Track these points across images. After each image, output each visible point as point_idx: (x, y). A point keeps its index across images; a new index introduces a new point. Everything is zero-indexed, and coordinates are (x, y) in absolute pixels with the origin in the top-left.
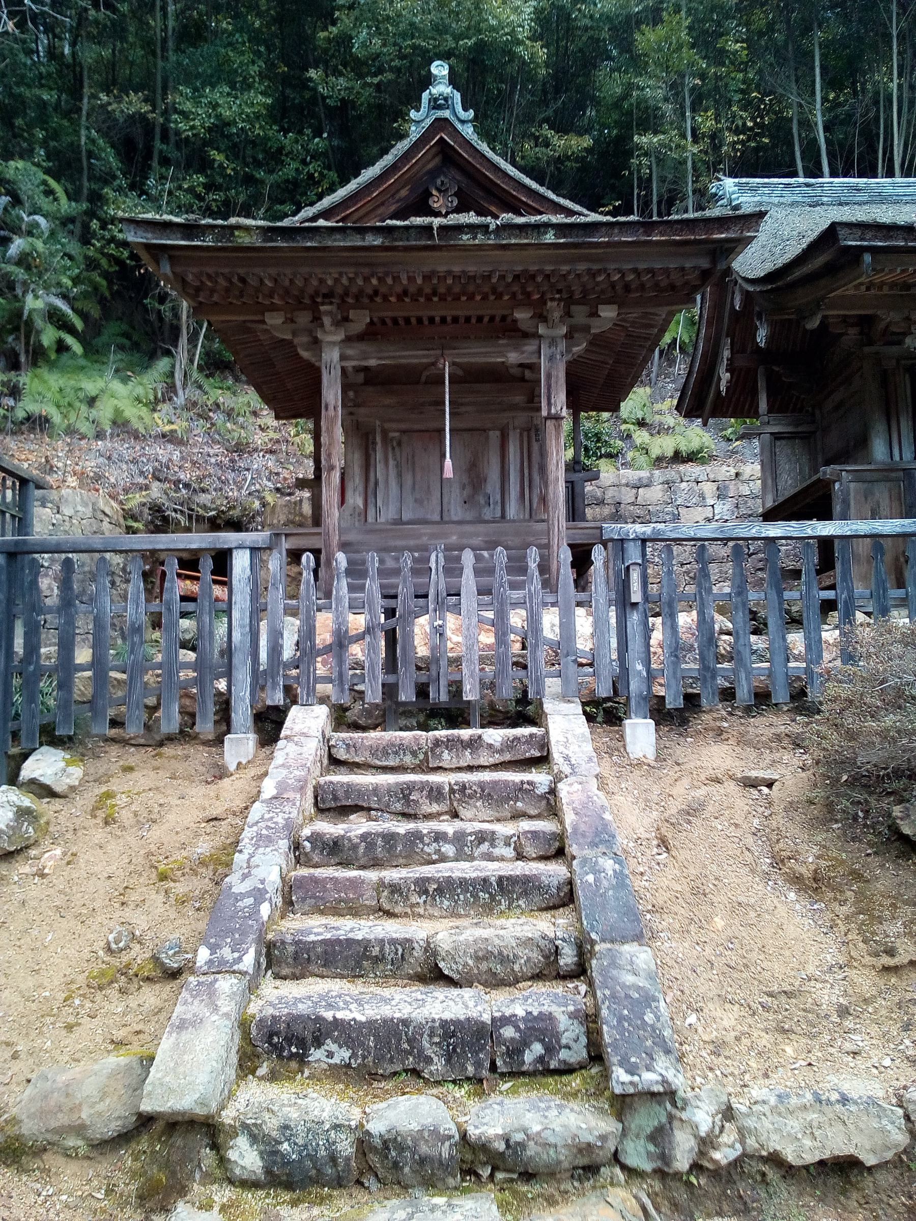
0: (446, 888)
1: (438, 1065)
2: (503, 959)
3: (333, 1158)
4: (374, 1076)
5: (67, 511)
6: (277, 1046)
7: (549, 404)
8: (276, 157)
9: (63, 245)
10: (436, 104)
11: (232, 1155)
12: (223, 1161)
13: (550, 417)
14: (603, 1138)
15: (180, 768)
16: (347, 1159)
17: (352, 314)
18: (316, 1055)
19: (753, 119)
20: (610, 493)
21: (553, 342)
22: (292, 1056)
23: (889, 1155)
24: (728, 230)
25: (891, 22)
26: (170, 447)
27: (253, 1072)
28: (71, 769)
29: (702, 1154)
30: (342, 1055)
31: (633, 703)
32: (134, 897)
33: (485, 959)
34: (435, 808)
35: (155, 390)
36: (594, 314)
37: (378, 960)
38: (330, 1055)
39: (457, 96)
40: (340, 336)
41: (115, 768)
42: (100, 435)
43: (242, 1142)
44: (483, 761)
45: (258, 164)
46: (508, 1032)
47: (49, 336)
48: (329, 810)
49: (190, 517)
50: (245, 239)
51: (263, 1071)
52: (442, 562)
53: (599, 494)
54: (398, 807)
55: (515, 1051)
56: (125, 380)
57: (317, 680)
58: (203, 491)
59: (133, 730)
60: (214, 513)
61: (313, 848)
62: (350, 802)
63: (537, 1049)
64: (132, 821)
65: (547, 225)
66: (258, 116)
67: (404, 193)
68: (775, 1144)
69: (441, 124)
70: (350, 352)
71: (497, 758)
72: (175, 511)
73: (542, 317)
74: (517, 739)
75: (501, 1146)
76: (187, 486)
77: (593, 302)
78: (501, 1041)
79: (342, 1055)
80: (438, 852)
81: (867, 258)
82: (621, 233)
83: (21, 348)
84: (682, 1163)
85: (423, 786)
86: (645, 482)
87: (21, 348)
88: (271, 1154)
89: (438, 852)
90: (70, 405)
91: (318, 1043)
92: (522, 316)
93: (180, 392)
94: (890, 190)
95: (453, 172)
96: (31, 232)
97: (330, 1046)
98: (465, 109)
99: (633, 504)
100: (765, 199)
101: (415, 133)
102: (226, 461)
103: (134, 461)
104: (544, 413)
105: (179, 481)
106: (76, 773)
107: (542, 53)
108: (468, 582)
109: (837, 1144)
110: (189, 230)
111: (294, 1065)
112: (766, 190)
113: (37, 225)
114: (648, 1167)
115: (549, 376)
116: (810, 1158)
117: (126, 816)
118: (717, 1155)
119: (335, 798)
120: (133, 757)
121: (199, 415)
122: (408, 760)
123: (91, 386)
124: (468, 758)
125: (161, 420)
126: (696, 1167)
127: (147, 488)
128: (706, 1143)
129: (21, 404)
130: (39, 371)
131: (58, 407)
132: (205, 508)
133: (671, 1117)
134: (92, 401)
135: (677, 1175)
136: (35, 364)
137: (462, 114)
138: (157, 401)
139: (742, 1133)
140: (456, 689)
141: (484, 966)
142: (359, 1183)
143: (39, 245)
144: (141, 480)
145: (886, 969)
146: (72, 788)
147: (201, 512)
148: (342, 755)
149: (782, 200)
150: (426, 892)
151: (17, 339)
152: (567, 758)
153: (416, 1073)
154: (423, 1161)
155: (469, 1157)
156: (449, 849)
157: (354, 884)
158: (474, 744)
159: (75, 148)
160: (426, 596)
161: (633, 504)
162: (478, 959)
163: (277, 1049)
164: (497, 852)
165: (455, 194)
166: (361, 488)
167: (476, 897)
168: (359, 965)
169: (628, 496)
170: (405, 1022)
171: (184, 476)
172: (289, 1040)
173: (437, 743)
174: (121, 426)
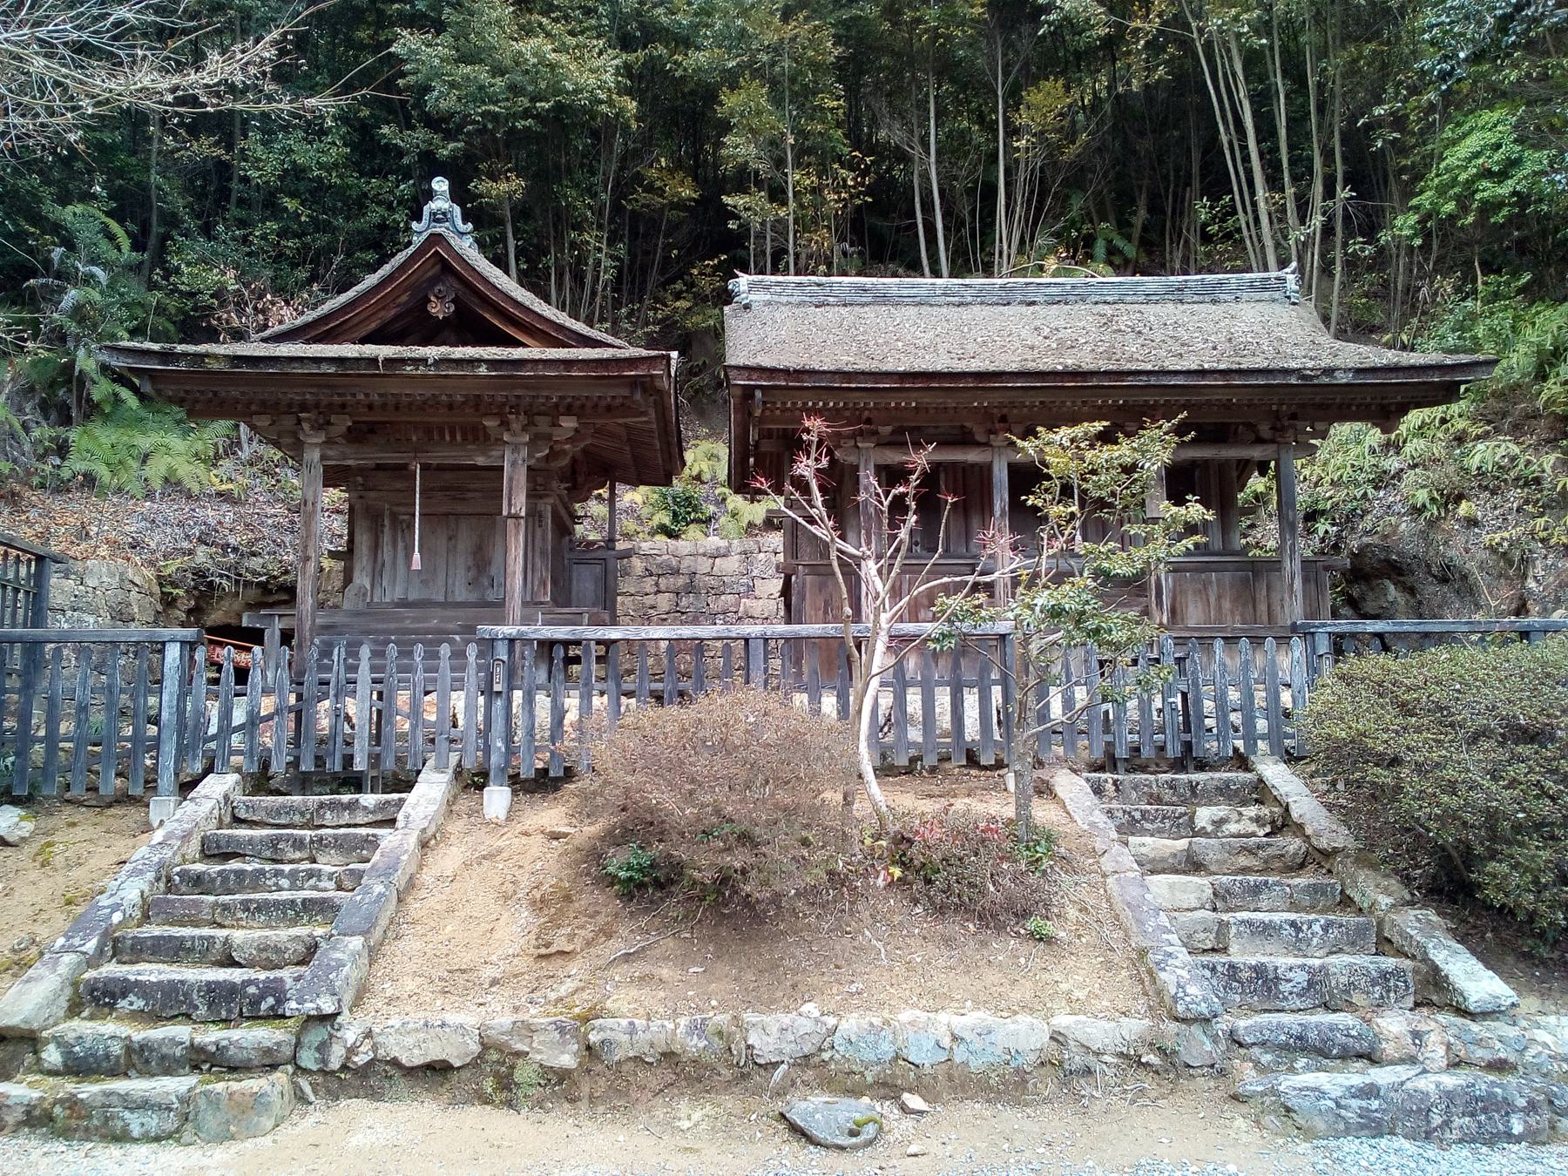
0: (262, 907)
1: (203, 1011)
2: (277, 950)
3: (107, 1056)
4: (160, 1018)
5: (91, 582)
6: (97, 998)
7: (510, 505)
8: (359, 204)
9: (121, 295)
10: (436, 218)
11: (44, 1055)
12: (39, 1060)
13: (510, 516)
14: (278, 1044)
15: (115, 824)
16: (118, 1057)
17: (333, 418)
18: (122, 1003)
19: (854, 179)
20: (686, 563)
21: (516, 449)
22: (106, 1004)
23: (468, 1060)
24: (636, 369)
25: (996, 79)
26: (225, 507)
27: (78, 1015)
28: (23, 824)
29: (348, 1058)
30: (139, 1004)
31: (492, 774)
32: (45, 916)
33: (265, 950)
34: (298, 855)
35: (216, 445)
36: (555, 424)
37: (191, 950)
38: (131, 1004)
39: (457, 210)
40: (321, 438)
41: (61, 824)
42: (149, 496)
43: (52, 1047)
44: (359, 820)
45: (335, 212)
46: (252, 990)
47: (101, 390)
48: (214, 856)
49: (237, 582)
50: (215, 366)
51: (85, 1014)
52: (343, 655)
53: (674, 562)
54: (268, 854)
55: (255, 1002)
56: (185, 434)
57: (232, 753)
58: (254, 554)
59: (77, 792)
60: (263, 579)
61: (181, 882)
62: (230, 850)
63: (271, 1001)
64: (63, 863)
65: (480, 361)
66: (336, 165)
67: (404, 298)
68: (394, 1052)
69: (437, 239)
70: (330, 453)
71: (371, 818)
72: (221, 576)
73: (505, 424)
74: (388, 802)
75: (214, 1049)
76: (235, 550)
77: (556, 412)
78: (245, 995)
79: (139, 1004)
80: (276, 884)
81: (758, 394)
82: (544, 369)
83: (72, 401)
84: (335, 1064)
85: (288, 838)
86: (722, 551)
87: (72, 401)
88: (68, 1053)
89: (276, 884)
90: (120, 462)
91: (124, 996)
92: (490, 423)
93: (245, 446)
94: (894, 291)
95: (451, 281)
96: (89, 280)
97: (132, 997)
98: (465, 221)
99: (708, 574)
100: (776, 298)
101: (417, 240)
102: (285, 522)
103: (181, 524)
104: (505, 513)
105: (228, 545)
106: (28, 827)
107: (632, 106)
108: (364, 674)
109: (435, 1053)
110: (165, 357)
111: (106, 1010)
112: (778, 289)
113: (93, 276)
114: (315, 1068)
115: (511, 479)
116: (417, 1062)
117: (59, 861)
118: (356, 1059)
119: (218, 847)
120: (80, 814)
121: (264, 471)
122: (297, 819)
123: (144, 442)
124: (346, 817)
125: (215, 480)
126: (344, 1068)
127: (191, 552)
128: (352, 1051)
129: (66, 463)
130: (90, 426)
131: (108, 465)
132: (254, 573)
133: (331, 1036)
134: (145, 458)
135: (333, 1072)
136: (87, 417)
137: (462, 227)
138: (217, 457)
139: (375, 1048)
140: (348, 760)
141: (264, 955)
142: (126, 1074)
143: (96, 296)
144: (185, 545)
145: (541, 956)
146: (23, 839)
147: (249, 577)
148: (242, 815)
149: (791, 299)
150: (248, 910)
151: (70, 390)
152: (407, 817)
153: (188, 1016)
154: (163, 1057)
155: (194, 1057)
156: (284, 883)
157: (196, 904)
158: (352, 807)
159: (144, 188)
160: (328, 684)
161: (708, 574)
162: (261, 951)
163: (96, 1000)
164: (322, 885)
165: (453, 301)
166: (369, 568)
167: (285, 914)
168: (176, 954)
169: (704, 565)
170: (182, 982)
171: (232, 540)
172: (105, 994)
173: (321, 805)
174: (172, 483)
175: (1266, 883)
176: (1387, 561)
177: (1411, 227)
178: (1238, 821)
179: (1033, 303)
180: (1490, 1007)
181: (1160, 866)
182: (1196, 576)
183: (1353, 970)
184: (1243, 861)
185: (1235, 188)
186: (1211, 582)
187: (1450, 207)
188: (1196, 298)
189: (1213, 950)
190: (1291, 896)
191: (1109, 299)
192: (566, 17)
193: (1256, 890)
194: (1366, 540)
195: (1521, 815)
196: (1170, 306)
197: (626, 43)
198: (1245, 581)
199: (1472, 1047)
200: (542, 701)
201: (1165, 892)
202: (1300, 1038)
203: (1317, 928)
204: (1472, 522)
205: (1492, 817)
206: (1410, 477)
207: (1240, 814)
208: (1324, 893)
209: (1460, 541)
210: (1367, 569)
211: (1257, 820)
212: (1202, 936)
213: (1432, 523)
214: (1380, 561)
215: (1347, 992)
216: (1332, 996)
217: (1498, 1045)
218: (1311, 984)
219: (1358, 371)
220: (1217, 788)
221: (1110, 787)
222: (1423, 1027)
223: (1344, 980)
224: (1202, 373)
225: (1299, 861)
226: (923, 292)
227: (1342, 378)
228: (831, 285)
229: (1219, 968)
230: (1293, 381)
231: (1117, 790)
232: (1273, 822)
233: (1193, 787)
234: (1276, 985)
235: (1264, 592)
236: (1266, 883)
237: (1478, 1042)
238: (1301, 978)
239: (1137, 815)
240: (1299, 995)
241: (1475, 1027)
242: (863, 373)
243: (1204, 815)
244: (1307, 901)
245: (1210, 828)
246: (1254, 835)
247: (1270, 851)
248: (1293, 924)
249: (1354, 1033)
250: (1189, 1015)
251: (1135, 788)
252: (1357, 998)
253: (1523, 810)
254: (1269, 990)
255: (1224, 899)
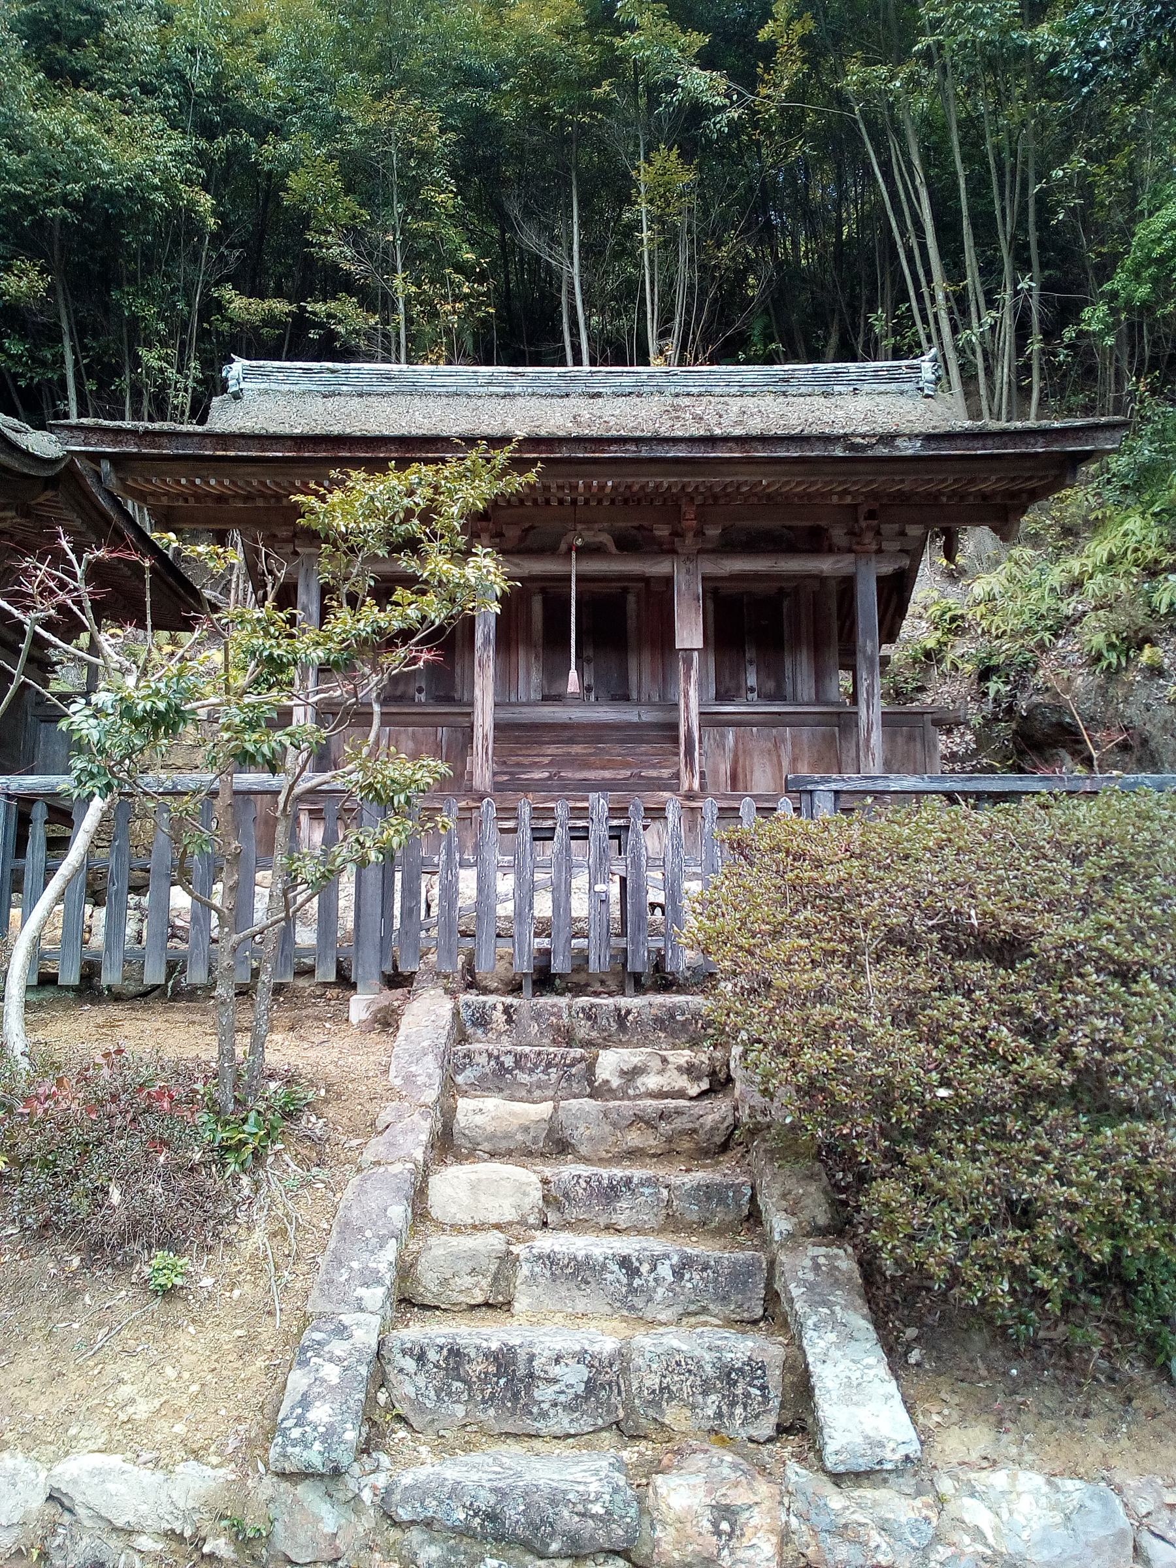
112: (280, 376)
175: (629, 1180)
176: (1060, 724)
177: (1100, 321)
178: (661, 1072)
179: (598, 395)
180: (863, 1464)
181: (503, 1145)
182: (766, 730)
183: (675, 1364)
184: (634, 1138)
185: (912, 293)
186: (784, 741)
187: (1143, 291)
188: (803, 390)
189: (487, 1305)
190: (669, 1203)
191: (694, 390)
192: (122, 96)
193: (610, 1193)
194: (1037, 699)
195: (943, 1092)
196: (769, 399)
197: (208, 131)
198: (830, 740)
199: (830, 1541)
200: (580, 907)
201: (464, 1196)
202: (492, 1517)
203: (665, 1270)
204: (1156, 671)
205: (884, 1099)
206: (1090, 621)
207: (664, 1060)
208: (722, 1201)
209: (1142, 695)
210: (1038, 735)
211: (690, 1070)
212: (468, 1281)
213: (1112, 673)
214: (1052, 725)
215: (655, 1404)
216: (631, 1411)
217: (876, 1538)
218: (591, 1387)
219: (929, 438)
220: (657, 1020)
221: (499, 1016)
222: (738, 1497)
223: (652, 1381)
224: (711, 440)
225: (719, 1140)
226: (460, 380)
227: (909, 449)
228: (347, 372)
229: (432, 1355)
230: (839, 452)
231: (509, 1021)
232: (713, 1074)
233: (621, 1017)
234: (528, 1388)
235: (853, 753)
236: (629, 1180)
237: (842, 1531)
238: (574, 1376)
239: (509, 1061)
240: (569, 1408)
241: (836, 1500)
242: (242, 436)
243: (610, 1063)
244: (693, 1213)
245: (615, 1082)
246: (681, 1094)
247: (679, 1123)
248: (624, 1262)
249: (597, 1509)
250: (289, 1468)
251: (537, 1016)
252: (673, 1415)
253: (945, 1083)
254: (516, 1396)
255: (560, 1209)
